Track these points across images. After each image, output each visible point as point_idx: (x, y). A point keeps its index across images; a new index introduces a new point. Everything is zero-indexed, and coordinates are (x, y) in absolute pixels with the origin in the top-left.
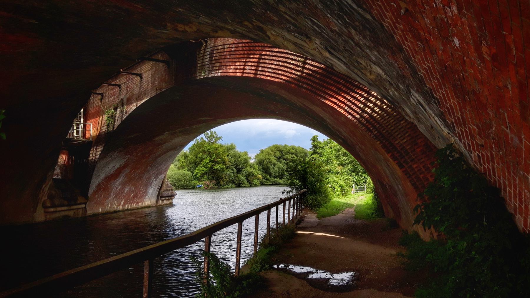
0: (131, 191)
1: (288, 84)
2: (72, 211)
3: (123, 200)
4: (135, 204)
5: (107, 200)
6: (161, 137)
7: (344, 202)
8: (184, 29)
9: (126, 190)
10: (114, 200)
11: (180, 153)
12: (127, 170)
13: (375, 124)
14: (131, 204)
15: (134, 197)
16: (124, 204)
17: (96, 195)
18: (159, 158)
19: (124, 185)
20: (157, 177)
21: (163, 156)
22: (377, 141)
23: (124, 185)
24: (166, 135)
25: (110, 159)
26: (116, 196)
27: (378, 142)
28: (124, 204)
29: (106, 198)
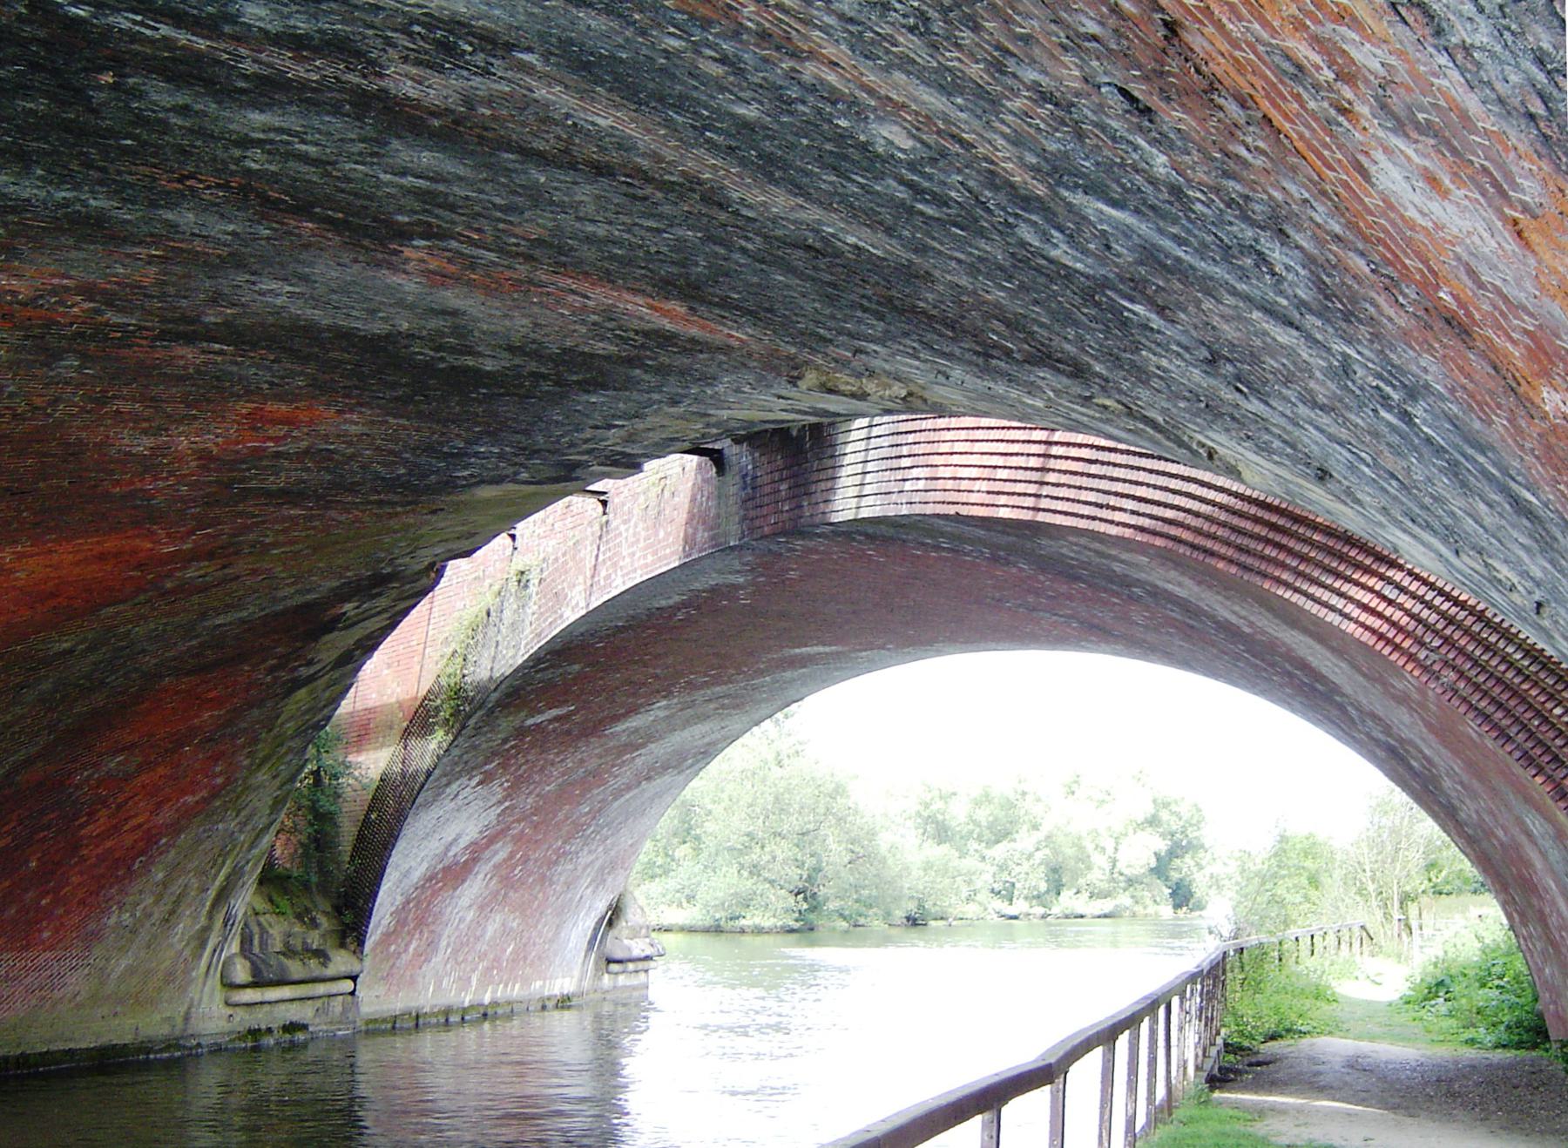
0: (505, 931)
1: (1188, 553)
2: (310, 1002)
3: (476, 968)
4: (517, 986)
5: (424, 968)
6: (635, 722)
7: (883, 842)
8: (860, 388)
9: (492, 928)
10: (449, 966)
11: (695, 783)
12: (501, 852)
13: (1525, 686)
14: (506, 986)
15: (514, 960)
16: (483, 985)
17: (390, 945)
18: (616, 804)
19: (485, 907)
20: (599, 881)
21: (631, 794)
22: (1534, 776)
23: (485, 907)
24: (659, 710)
25: (452, 804)
26: (456, 952)
27: (1539, 780)
28: (483, 985)
29: (423, 956)
